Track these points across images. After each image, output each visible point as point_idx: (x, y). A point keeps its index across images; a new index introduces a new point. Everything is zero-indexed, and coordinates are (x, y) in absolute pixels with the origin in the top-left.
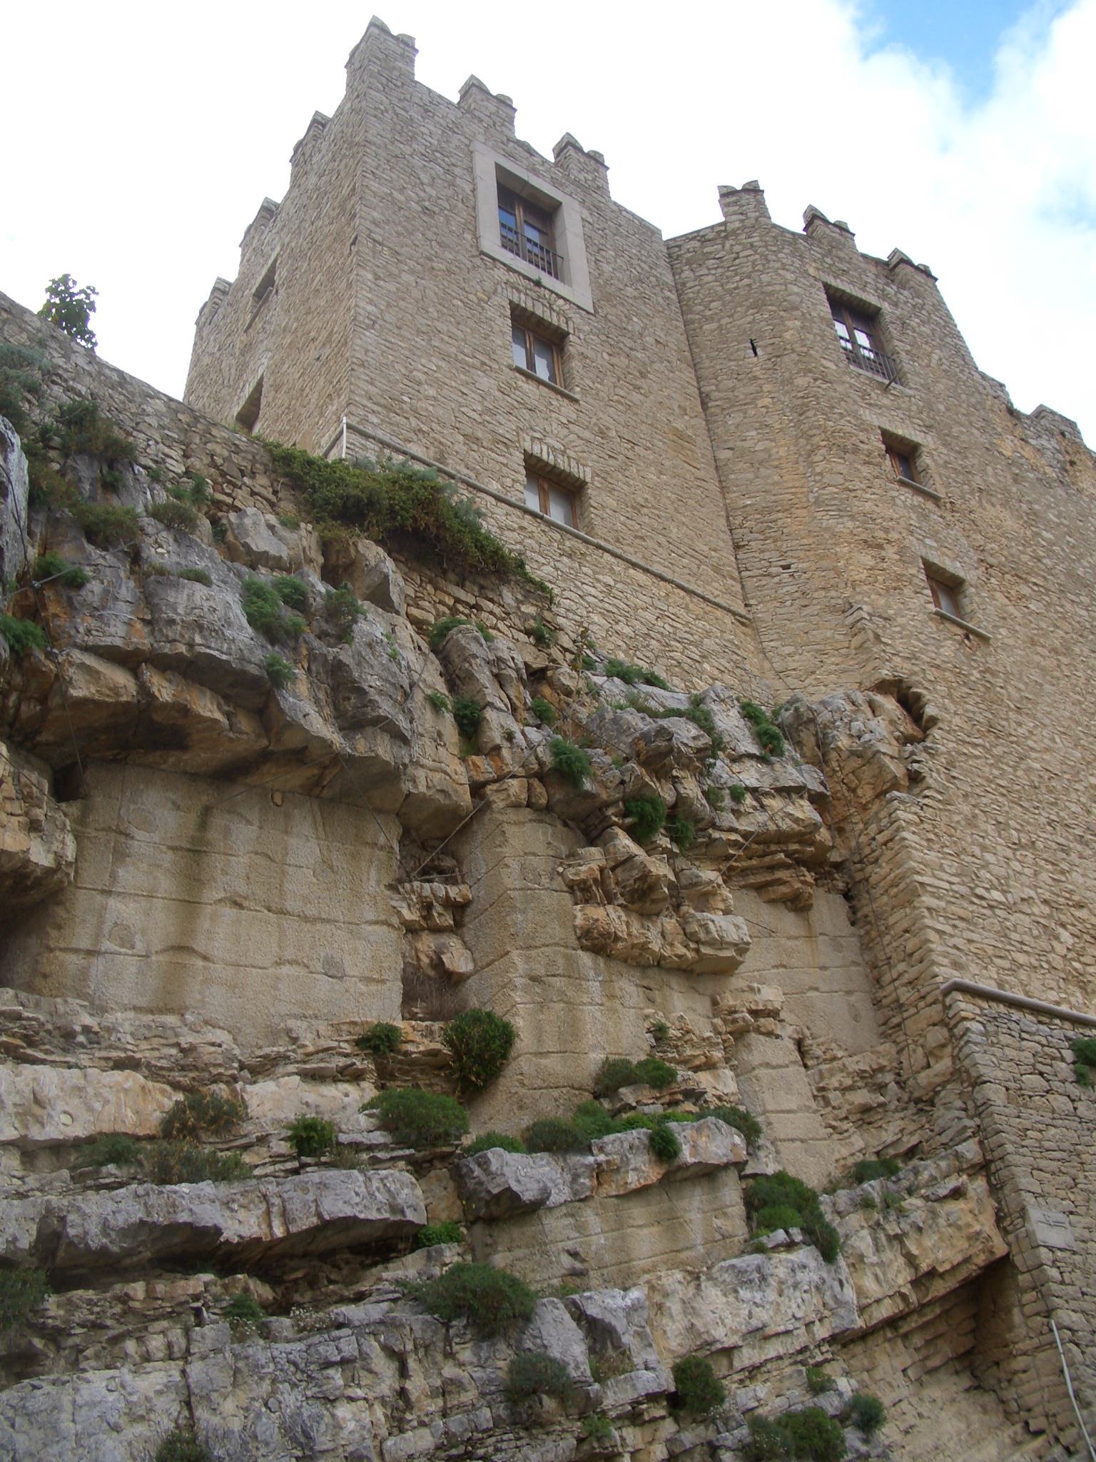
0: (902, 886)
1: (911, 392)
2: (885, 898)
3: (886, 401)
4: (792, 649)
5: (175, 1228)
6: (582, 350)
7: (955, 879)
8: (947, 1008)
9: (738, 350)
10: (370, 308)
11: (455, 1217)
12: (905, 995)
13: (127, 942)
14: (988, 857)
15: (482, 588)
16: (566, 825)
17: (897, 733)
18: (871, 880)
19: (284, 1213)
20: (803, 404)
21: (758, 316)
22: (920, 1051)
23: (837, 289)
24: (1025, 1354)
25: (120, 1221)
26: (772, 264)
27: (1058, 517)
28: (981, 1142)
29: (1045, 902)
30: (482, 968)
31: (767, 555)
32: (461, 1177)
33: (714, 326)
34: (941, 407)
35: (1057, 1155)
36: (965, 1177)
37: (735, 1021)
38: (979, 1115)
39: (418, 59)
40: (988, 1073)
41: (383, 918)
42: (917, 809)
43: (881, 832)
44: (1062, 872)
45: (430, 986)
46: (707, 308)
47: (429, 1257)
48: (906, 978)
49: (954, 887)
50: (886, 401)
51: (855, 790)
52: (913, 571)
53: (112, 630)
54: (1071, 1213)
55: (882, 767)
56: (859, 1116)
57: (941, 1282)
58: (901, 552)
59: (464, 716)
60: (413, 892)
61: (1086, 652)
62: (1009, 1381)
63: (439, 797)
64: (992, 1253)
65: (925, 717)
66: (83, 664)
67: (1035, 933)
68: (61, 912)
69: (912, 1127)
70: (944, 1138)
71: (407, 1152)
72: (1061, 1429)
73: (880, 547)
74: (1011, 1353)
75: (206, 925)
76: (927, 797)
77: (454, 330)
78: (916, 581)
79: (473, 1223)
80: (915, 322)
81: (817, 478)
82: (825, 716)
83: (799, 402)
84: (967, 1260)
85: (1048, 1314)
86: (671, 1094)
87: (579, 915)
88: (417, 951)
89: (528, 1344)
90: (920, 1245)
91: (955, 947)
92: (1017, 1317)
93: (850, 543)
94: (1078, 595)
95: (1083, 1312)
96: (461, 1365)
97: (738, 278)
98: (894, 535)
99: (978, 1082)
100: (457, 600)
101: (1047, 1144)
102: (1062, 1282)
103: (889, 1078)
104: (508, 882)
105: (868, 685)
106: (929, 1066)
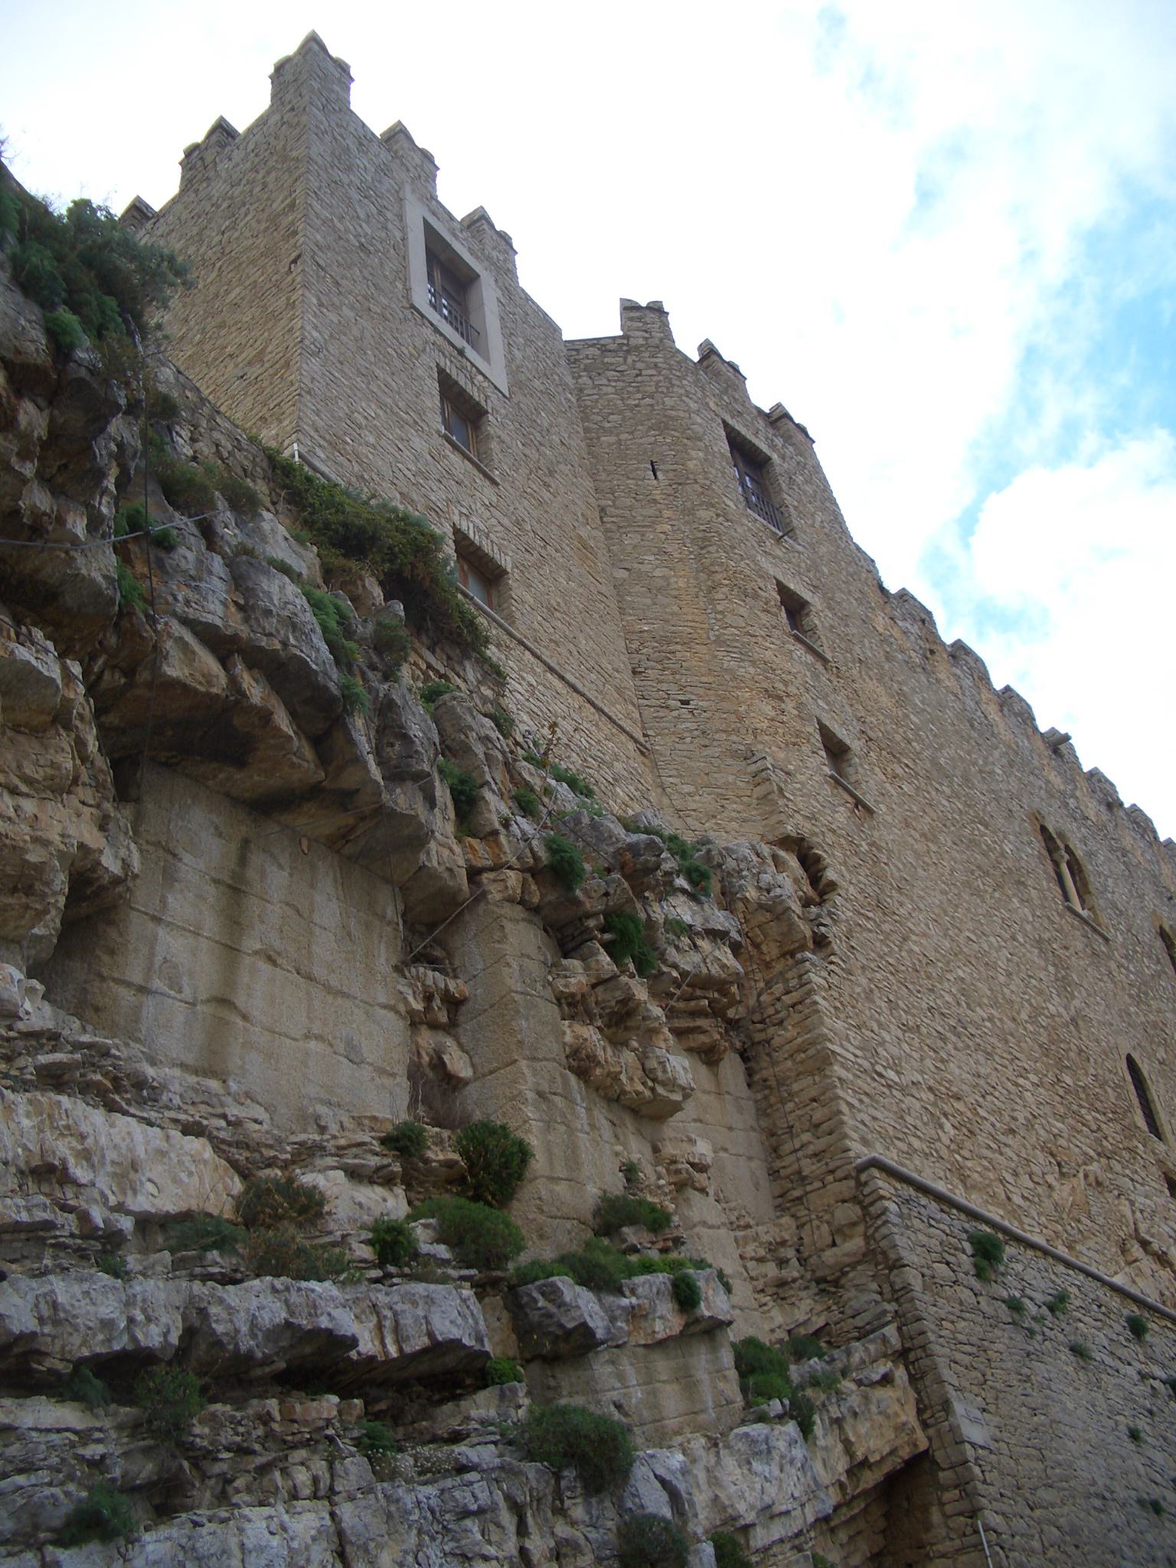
0: (812, 1052)
1: (800, 548)
2: (789, 1063)
3: (778, 552)
4: (691, 789)
5: (316, 1333)
6: (500, 433)
9: (637, 469)
10: (316, 334)
11: (511, 1353)
12: (809, 1167)
13: (175, 985)
14: (884, 1034)
15: (449, 658)
16: (545, 930)
19: (396, 1329)
20: (704, 539)
21: (660, 439)
22: (825, 1228)
23: (734, 429)
24: (944, 1556)
25: (266, 1319)
26: (675, 389)
27: (922, 702)
28: (899, 1329)
29: (930, 1089)
30: (484, 1076)
31: (665, 687)
32: (520, 1307)
33: (613, 439)
34: (825, 570)
35: (968, 1348)
37: (678, 1172)
38: (897, 1300)
39: (354, 88)
40: (909, 1257)
41: (392, 1002)
43: (787, 993)
44: (942, 1061)
45: (434, 1084)
46: (605, 419)
47: (502, 1396)
48: (811, 1149)
49: (859, 1061)
50: (778, 552)
51: (784, 942)
52: (811, 730)
53: (212, 607)
54: (984, 1410)
55: (791, 925)
56: (775, 1290)
57: (869, 1473)
58: (800, 706)
59: (461, 793)
60: (418, 978)
63: (446, 875)
65: (824, 881)
66: (181, 638)
68: (113, 933)
69: (819, 1308)
70: (859, 1322)
71: (473, 1272)
73: (780, 698)
74: (927, 1555)
75: (246, 980)
76: (832, 963)
77: (389, 380)
78: (813, 740)
79: (528, 1361)
80: (799, 479)
81: (719, 616)
82: (730, 864)
83: (700, 535)
84: (893, 1452)
86: (665, 1240)
87: (568, 1031)
88: (417, 1044)
89: (629, 1505)
90: (855, 1432)
91: (863, 1122)
92: (936, 1517)
93: (752, 690)
94: (941, 784)
95: (1003, 1514)
96: (573, 1523)
97: (639, 396)
98: (792, 690)
99: (898, 1265)
100: (429, 666)
101: (961, 1337)
102: (984, 1482)
103: (790, 1253)
104: (510, 982)
105: (771, 838)
106: (834, 1244)
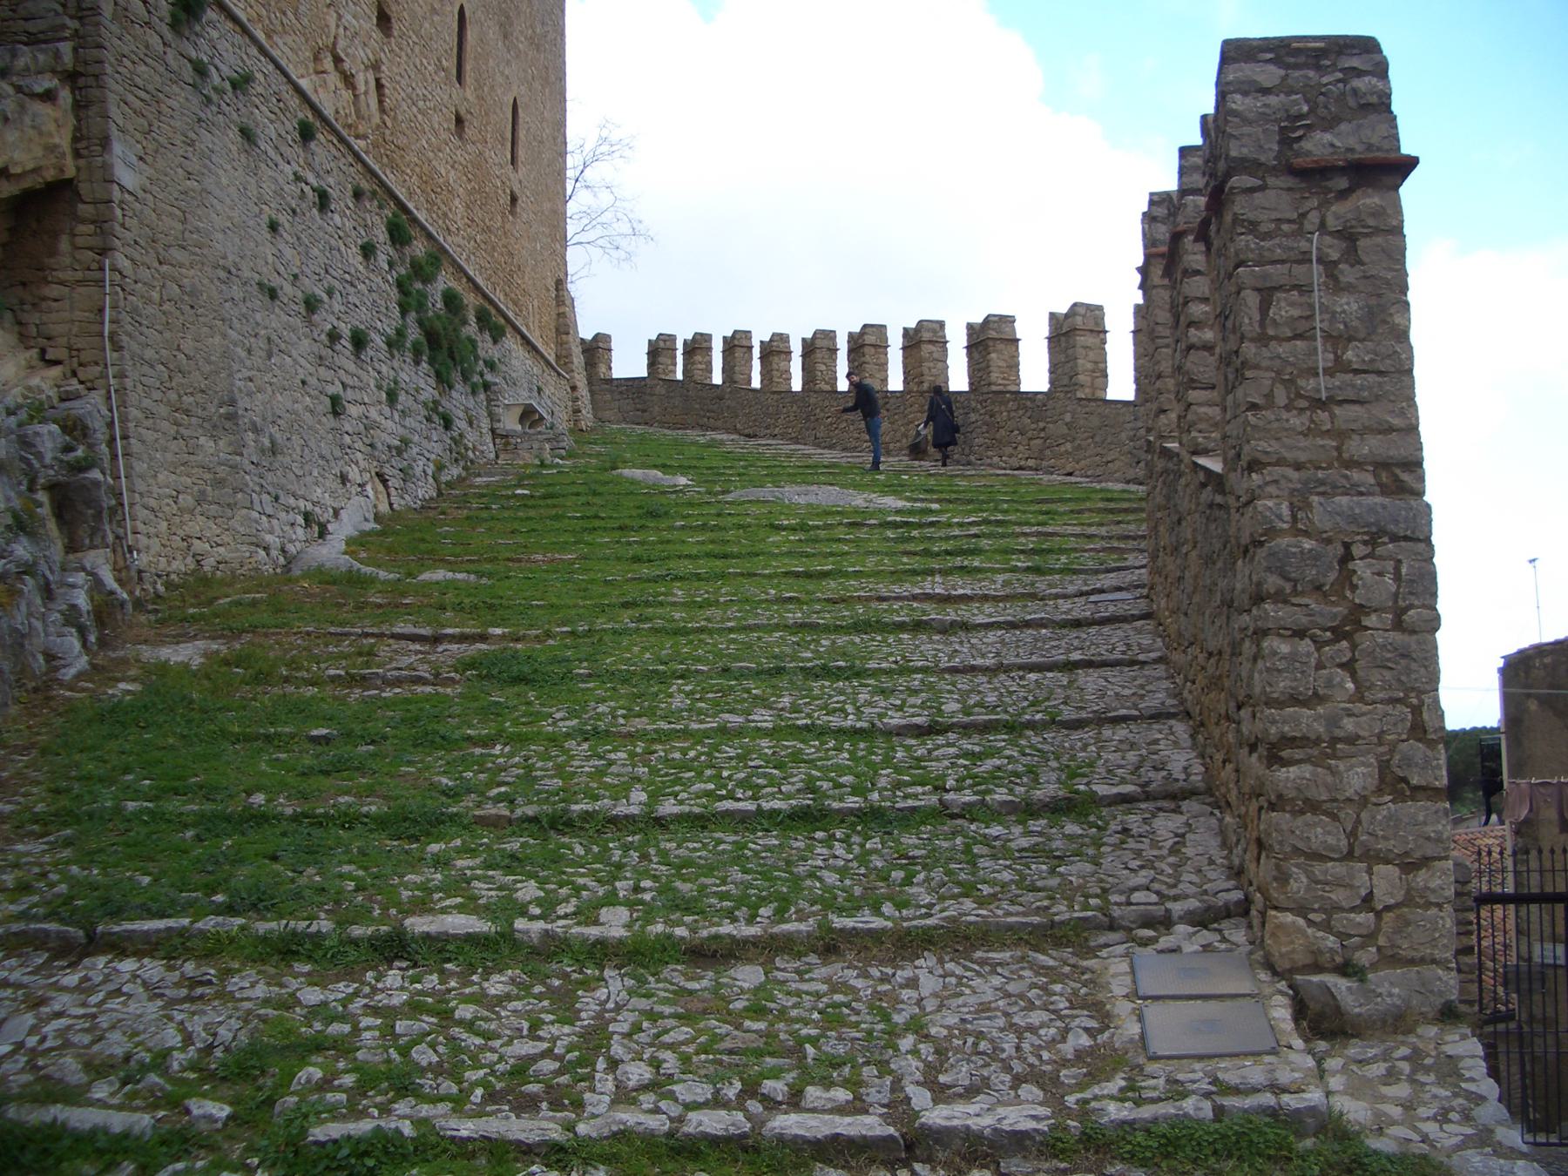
24: (61, 283)
28: (75, 50)
35: (143, 94)
38: (80, 19)
64: (62, 171)
70: (31, 27)
72: (81, 365)
74: (45, 278)
85: (104, 251)
92: (64, 244)
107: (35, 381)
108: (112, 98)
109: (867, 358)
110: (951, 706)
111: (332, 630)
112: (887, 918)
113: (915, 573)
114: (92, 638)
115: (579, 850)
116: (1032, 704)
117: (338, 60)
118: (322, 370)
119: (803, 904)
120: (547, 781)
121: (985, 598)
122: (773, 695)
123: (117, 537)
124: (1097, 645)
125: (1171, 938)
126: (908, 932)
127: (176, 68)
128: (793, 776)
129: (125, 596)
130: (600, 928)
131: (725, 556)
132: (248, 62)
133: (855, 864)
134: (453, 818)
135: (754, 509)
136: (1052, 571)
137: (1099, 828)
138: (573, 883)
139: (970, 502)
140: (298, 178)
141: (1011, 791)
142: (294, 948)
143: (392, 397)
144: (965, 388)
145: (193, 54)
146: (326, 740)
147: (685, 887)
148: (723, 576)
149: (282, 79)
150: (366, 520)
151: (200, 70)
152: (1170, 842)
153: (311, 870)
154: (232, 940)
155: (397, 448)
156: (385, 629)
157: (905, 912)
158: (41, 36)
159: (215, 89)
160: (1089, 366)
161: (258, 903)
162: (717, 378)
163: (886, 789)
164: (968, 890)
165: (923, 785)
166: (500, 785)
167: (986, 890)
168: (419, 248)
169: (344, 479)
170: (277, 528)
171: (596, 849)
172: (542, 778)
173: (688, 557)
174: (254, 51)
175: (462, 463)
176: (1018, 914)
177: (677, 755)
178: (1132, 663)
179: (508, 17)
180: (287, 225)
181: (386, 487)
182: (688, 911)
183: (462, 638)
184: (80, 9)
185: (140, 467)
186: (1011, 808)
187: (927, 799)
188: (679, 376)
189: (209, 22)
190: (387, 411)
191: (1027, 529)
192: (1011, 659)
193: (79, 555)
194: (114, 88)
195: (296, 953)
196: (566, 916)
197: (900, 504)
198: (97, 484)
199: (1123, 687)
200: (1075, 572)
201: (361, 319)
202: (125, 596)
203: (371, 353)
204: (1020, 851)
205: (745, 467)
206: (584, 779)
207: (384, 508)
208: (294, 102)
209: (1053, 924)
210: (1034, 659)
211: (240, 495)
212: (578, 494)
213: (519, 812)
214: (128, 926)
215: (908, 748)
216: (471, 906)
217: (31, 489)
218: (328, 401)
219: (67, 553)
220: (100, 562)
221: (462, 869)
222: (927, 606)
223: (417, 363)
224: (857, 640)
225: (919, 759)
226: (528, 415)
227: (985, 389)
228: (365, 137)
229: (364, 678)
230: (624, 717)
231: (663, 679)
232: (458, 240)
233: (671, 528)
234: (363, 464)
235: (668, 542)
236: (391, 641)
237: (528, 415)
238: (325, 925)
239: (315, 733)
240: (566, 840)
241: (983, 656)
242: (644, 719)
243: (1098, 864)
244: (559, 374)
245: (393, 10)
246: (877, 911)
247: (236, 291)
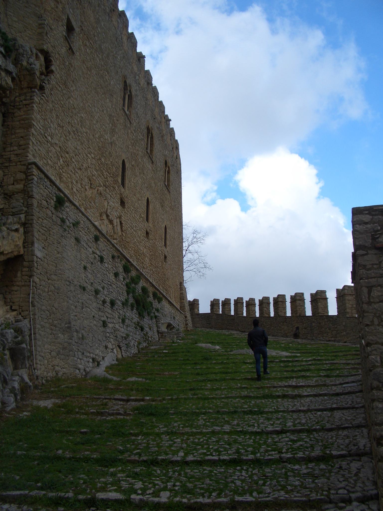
0: (26, 122)
7: (41, 127)
8: (28, 169)
12: (13, 158)
14: (52, 125)
17: (41, 70)
18: (15, 114)
22: (12, 178)
24: (18, 286)
27: (104, 25)
28: (25, 216)
29: (60, 147)
35: (45, 229)
36: (19, 226)
38: (28, 207)
40: (36, 196)
42: (39, 98)
43: (25, 100)
44: (67, 140)
52: (64, 18)
61: (95, 74)
62: (9, 293)
64: (19, 252)
65: (50, 69)
67: (55, 156)
70: (14, 210)
72: (22, 311)
74: (13, 284)
82: (21, 51)
84: (12, 252)
85: (31, 276)
91: (35, 150)
92: (19, 274)
94: (99, 54)
95: (39, 279)
99: (31, 197)
107: (8, 316)
108: (35, 230)
109: (280, 306)
110: (290, 424)
111: (95, 397)
112: (254, 497)
113: (287, 378)
114: (19, 398)
115: (159, 472)
116: (317, 423)
117: (108, 216)
118: (100, 313)
119: (227, 492)
120: (153, 448)
121: (309, 386)
122: (232, 420)
123: (30, 365)
124: (342, 402)
125: (351, 507)
126: (260, 502)
127: (56, 221)
128: (233, 448)
129: (31, 384)
130: (159, 499)
131: (226, 373)
132: (78, 218)
133: (248, 478)
134: (120, 460)
135: (239, 357)
136: (333, 376)
137: (332, 466)
138: (154, 483)
139: (310, 353)
140: (93, 253)
141: (304, 454)
142: (59, 502)
143: (123, 321)
144: (311, 315)
145: (61, 216)
146: (85, 433)
147: (190, 485)
148: (224, 380)
149: (89, 222)
150: (113, 360)
151: (63, 221)
152: (355, 472)
153: (70, 476)
154: (40, 499)
155: (125, 337)
156: (112, 397)
157: (260, 495)
158: (16, 213)
159: (67, 226)
160: (350, 306)
161: (51, 487)
162: (232, 313)
163: (262, 452)
164: (283, 488)
165: (274, 451)
166: (138, 449)
167: (289, 488)
168: (133, 273)
169: (106, 347)
170: (83, 363)
171: (164, 471)
172: (152, 447)
173: (215, 373)
174: (80, 214)
175: (147, 342)
176: (299, 497)
177: (197, 440)
178: (353, 408)
179: (163, 201)
180: (89, 267)
181: (121, 350)
182: (189, 493)
183: (136, 400)
184: (28, 205)
185: (39, 343)
186: (303, 459)
187: (275, 455)
188: (221, 312)
189: (67, 207)
190: (122, 325)
191: (327, 362)
192: (312, 407)
193: (18, 371)
194: (36, 227)
195: (60, 504)
196: (149, 494)
197: (287, 354)
198: (24, 348)
199: (348, 416)
200: (341, 376)
201: (114, 296)
202: (31, 384)
203: (116, 307)
204: (303, 474)
205: (239, 343)
206: (165, 448)
207: (120, 356)
208: (93, 229)
209: (310, 500)
210: (320, 407)
211: (71, 352)
212: (183, 352)
213: (141, 459)
214: (9, 493)
215: (273, 439)
216: (119, 490)
217: (4, 350)
218: (102, 323)
219: (14, 370)
220: (24, 373)
221: (119, 477)
222: (289, 389)
223: (132, 310)
224: (263, 401)
225: (276, 442)
226: (169, 326)
227: (317, 315)
228: (116, 239)
229: (102, 413)
230: (182, 427)
231: (198, 414)
232: (147, 270)
233: (211, 363)
234: (113, 342)
235: (209, 368)
236: (113, 401)
237: (169, 326)
238: (71, 495)
239: (82, 430)
240: (155, 468)
241: (304, 406)
242: (189, 428)
243: (329, 479)
244: (181, 313)
245: (126, 200)
246: (251, 495)
247: (72, 288)
